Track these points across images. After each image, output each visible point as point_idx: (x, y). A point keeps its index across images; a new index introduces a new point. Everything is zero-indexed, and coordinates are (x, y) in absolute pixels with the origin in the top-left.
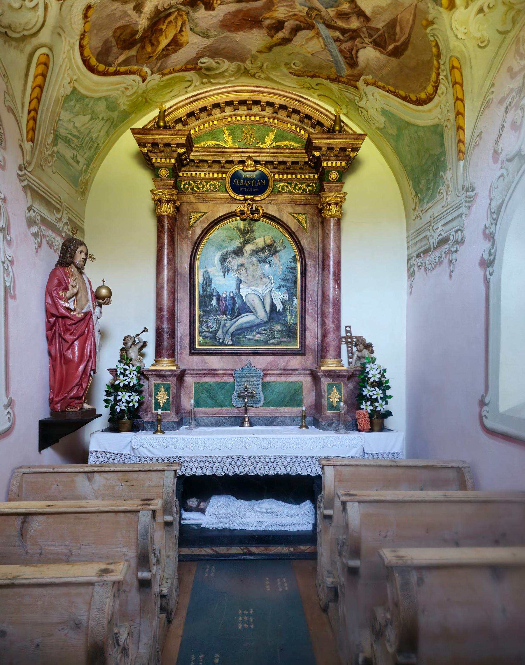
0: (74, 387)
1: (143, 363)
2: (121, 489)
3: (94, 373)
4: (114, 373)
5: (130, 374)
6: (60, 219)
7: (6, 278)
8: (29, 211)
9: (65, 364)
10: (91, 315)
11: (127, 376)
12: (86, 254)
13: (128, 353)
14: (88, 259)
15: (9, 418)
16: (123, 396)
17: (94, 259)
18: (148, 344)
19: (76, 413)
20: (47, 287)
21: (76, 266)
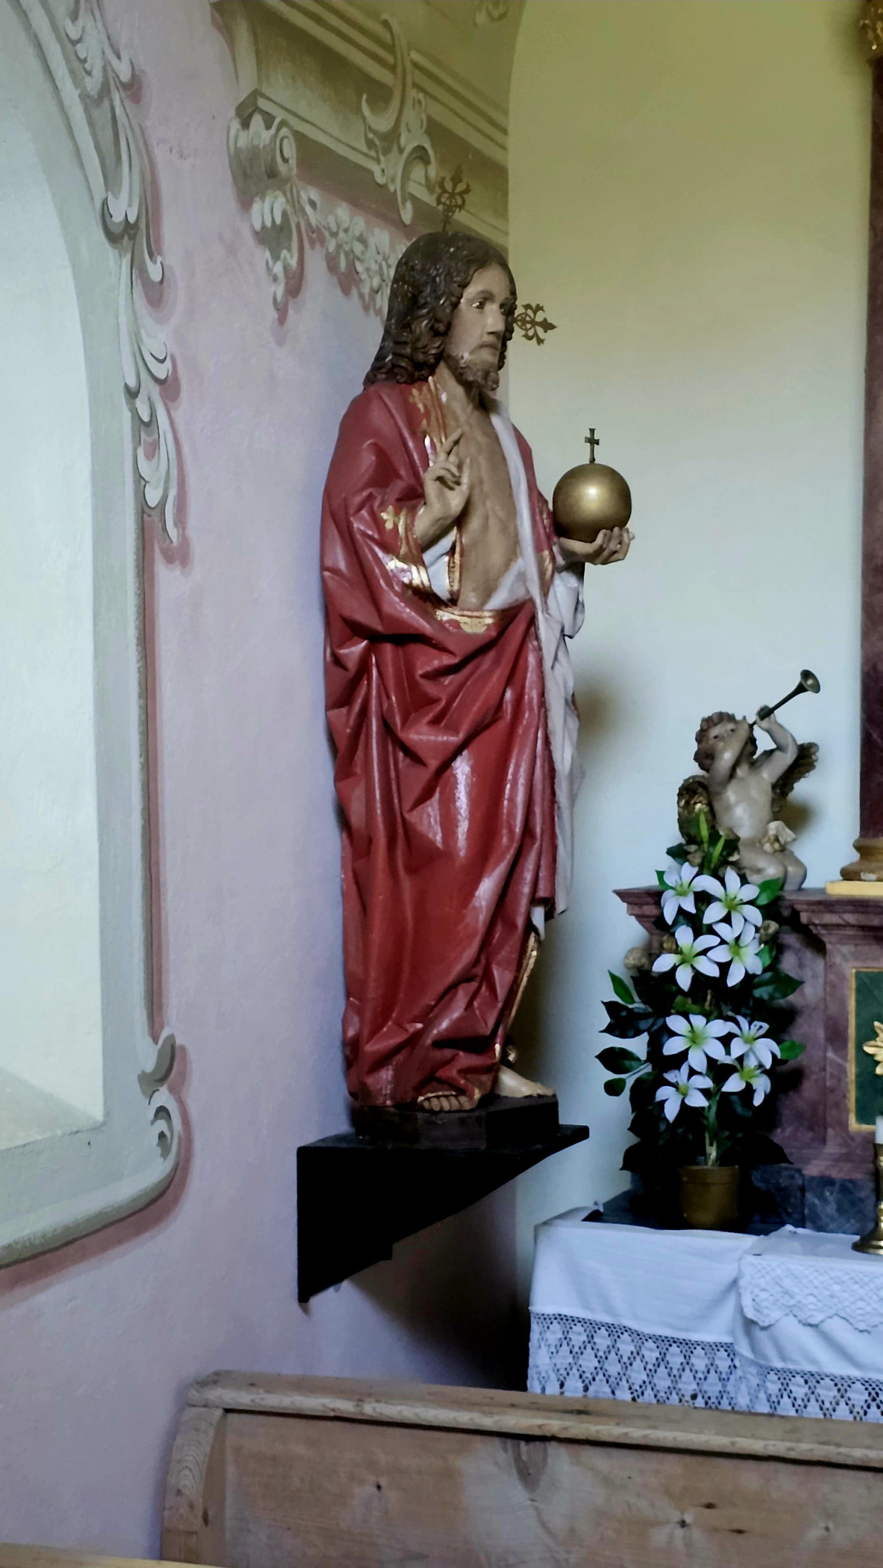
0: (453, 987)
1: (798, 863)
2: (679, 1542)
3: (549, 916)
4: (651, 910)
5: (727, 920)
6: (391, 138)
7: (145, 468)
8: (246, 124)
9: (412, 870)
10: (532, 621)
11: (711, 931)
12: (508, 309)
13: (717, 806)
14: (518, 332)
15: (162, 1135)
16: (695, 1038)
17: (547, 326)
18: (821, 755)
19: (462, 1122)
20: (328, 494)
21: (460, 377)
